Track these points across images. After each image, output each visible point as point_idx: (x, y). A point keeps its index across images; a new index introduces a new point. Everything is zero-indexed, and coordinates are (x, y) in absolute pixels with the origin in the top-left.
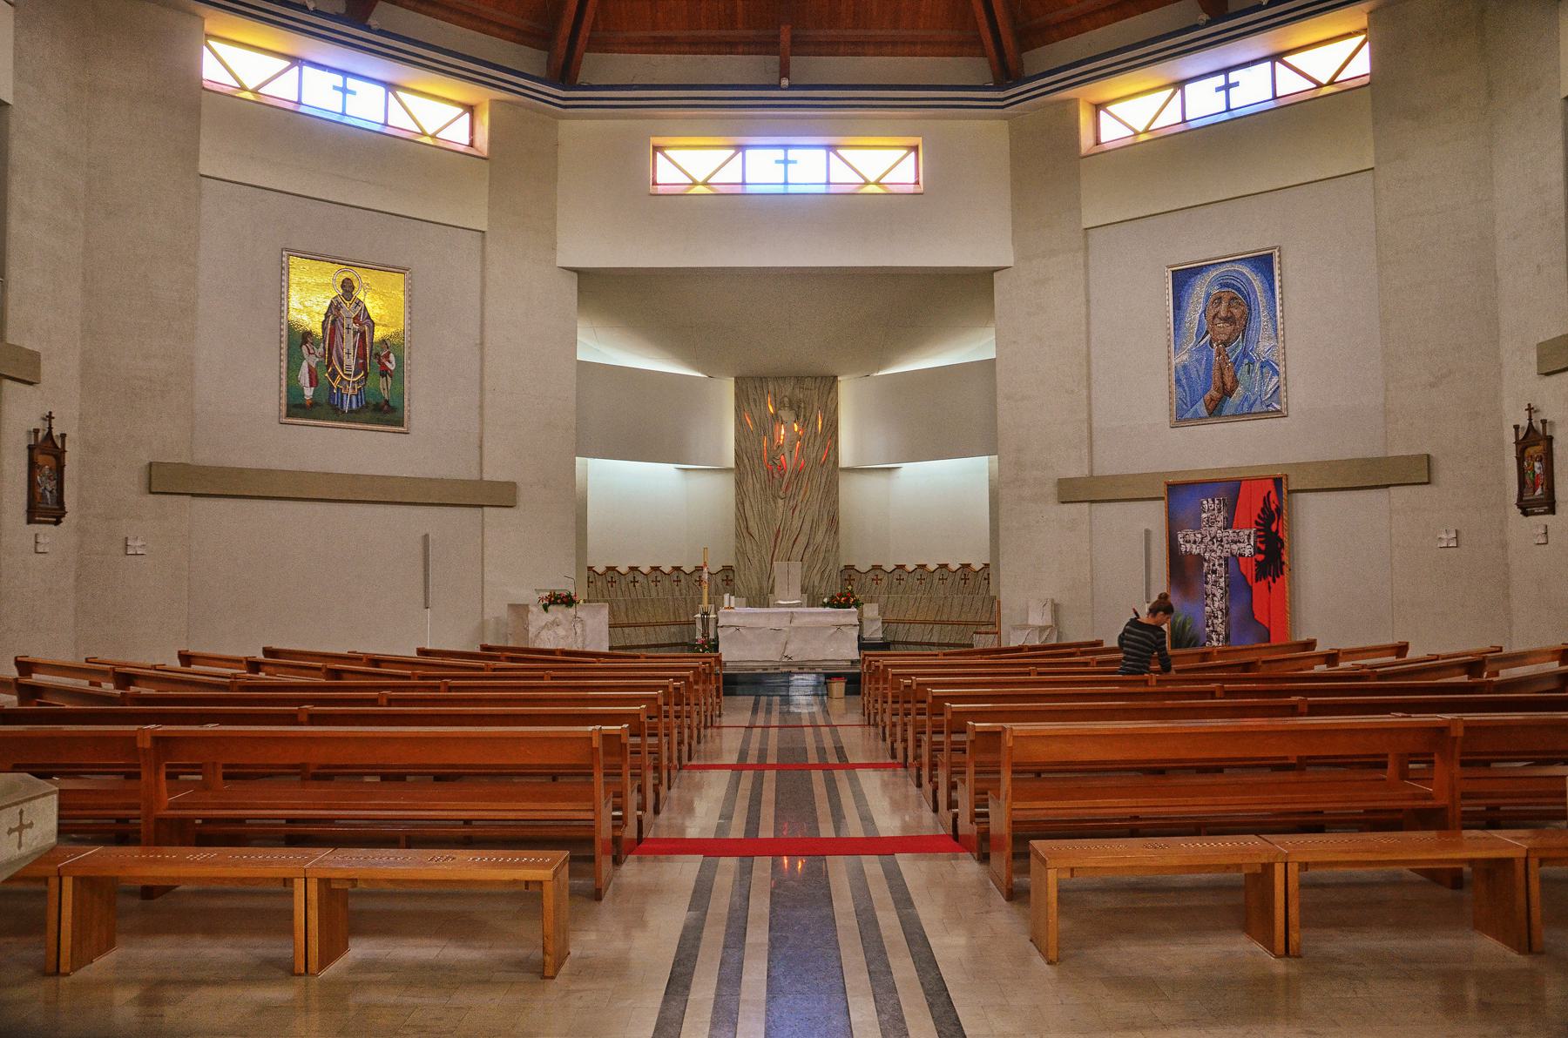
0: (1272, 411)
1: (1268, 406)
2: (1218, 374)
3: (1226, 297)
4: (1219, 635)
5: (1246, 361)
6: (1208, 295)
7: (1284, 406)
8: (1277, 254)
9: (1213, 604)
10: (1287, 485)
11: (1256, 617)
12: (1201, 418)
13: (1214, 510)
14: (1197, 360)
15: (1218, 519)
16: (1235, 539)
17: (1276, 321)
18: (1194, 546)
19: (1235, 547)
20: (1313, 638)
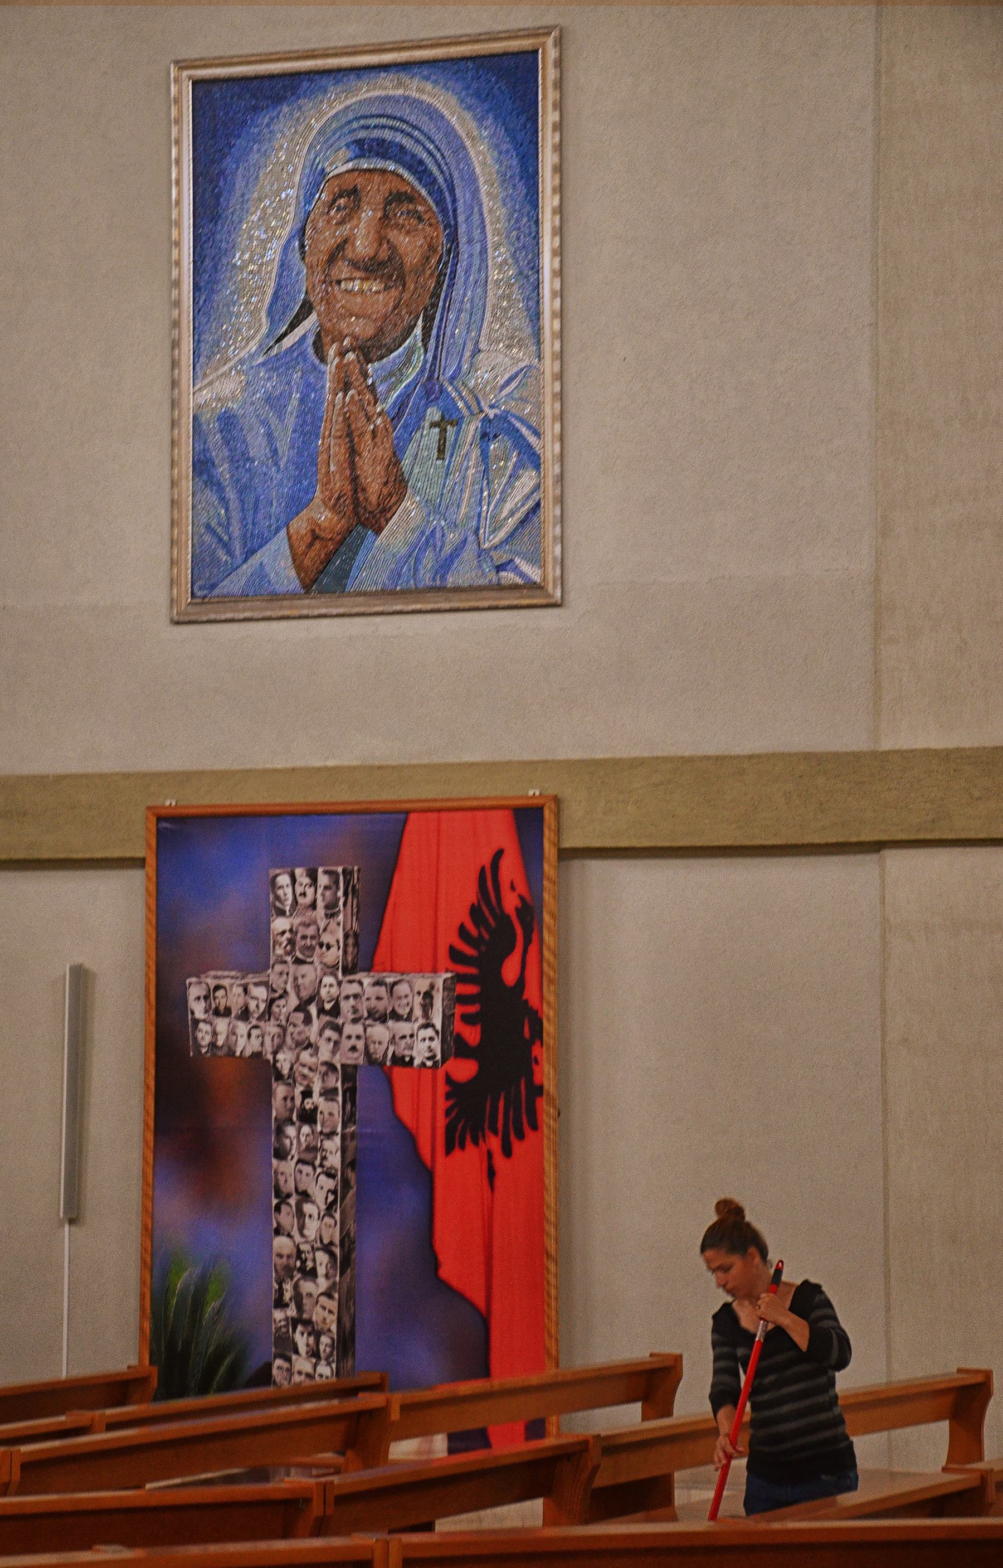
0: (515, 587)
1: (499, 568)
2: (338, 451)
3: (375, 192)
4: (317, 1334)
5: (433, 414)
6: (318, 178)
7: (553, 572)
8: (552, 54)
9: (301, 1228)
10: (558, 832)
11: (445, 1272)
12: (275, 597)
13: (313, 906)
14: (268, 399)
15: (326, 938)
16: (381, 1006)
17: (537, 286)
18: (242, 1028)
19: (379, 1032)
20: (676, 1351)
